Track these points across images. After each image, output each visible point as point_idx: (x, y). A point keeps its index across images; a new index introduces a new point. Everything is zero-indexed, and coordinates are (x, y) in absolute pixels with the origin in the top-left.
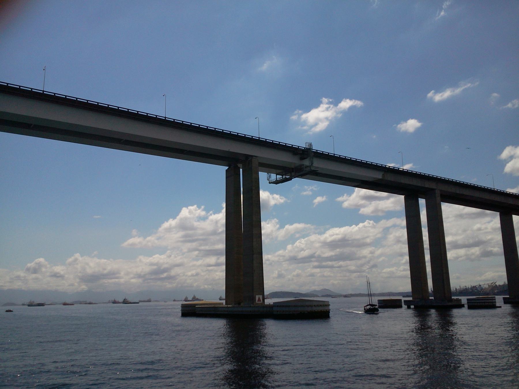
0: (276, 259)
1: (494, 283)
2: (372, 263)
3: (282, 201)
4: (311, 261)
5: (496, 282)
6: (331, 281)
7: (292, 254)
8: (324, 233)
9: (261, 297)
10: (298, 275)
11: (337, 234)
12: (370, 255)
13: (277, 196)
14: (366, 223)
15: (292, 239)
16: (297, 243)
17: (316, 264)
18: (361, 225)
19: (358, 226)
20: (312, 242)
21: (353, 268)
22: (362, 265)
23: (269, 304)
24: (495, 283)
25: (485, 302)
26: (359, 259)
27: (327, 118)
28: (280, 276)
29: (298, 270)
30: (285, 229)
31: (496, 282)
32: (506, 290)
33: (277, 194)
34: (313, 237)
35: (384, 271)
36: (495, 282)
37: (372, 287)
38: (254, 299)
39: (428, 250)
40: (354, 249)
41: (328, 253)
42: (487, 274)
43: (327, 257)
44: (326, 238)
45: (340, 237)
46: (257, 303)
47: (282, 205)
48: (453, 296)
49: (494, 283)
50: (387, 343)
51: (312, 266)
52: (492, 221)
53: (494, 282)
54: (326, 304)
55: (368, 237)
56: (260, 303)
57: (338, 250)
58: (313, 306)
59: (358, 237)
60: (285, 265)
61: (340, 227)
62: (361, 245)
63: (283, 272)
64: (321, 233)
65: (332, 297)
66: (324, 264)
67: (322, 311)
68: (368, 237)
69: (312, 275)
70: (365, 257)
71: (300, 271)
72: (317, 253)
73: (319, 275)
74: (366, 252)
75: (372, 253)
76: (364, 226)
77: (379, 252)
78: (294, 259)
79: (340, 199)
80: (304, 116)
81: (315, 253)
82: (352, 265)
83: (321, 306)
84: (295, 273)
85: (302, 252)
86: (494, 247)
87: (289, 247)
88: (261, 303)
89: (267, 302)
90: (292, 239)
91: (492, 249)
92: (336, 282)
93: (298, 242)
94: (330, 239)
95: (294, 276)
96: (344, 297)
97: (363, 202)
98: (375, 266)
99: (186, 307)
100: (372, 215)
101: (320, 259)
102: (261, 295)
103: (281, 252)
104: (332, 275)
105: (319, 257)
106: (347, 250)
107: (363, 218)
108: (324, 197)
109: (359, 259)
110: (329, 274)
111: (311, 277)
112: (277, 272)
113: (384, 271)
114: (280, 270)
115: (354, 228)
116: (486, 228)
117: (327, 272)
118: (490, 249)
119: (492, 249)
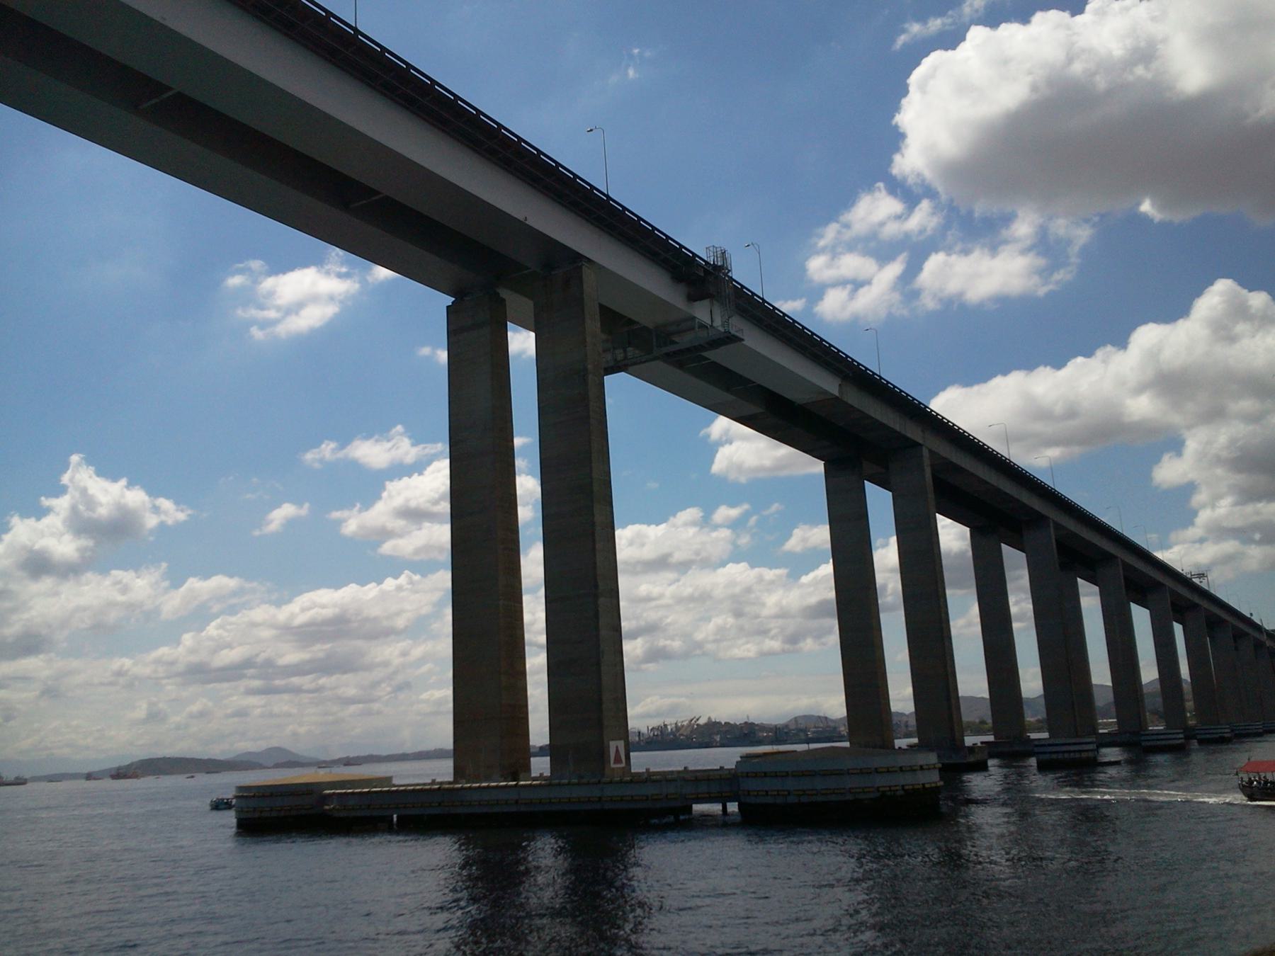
0: (147, 671)
1: (695, 720)
2: (400, 678)
3: (181, 516)
4: (242, 677)
5: (700, 717)
6: (291, 727)
7: (194, 659)
8: (289, 601)
9: (621, 744)
10: (202, 714)
11: (323, 607)
12: (402, 659)
13: (166, 504)
14: (403, 580)
15: (199, 616)
16: (212, 630)
17: (257, 683)
18: (390, 583)
19: (381, 586)
20: (254, 625)
21: (351, 692)
22: (375, 685)
23: (681, 769)
24: (698, 720)
25: (1080, 751)
26: (369, 668)
27: (331, 298)
28: (154, 716)
29: (204, 700)
30: (182, 589)
31: (700, 717)
32: (746, 734)
33: (167, 497)
34: (260, 613)
35: (424, 696)
36: (697, 717)
37: (750, 718)
38: (602, 754)
39: (532, 644)
40: (360, 643)
41: (292, 656)
42: (649, 700)
43: (286, 667)
44: (293, 616)
45: (328, 613)
46: (613, 769)
47: (179, 526)
48: (632, 751)
49: (695, 720)
50: (682, 884)
51: (242, 689)
52: (678, 580)
53: (695, 717)
54: (921, 763)
55: (398, 614)
56: (619, 768)
57: (318, 647)
58: (915, 770)
59: (375, 612)
60: (170, 688)
61: (337, 586)
62: (381, 632)
63: (161, 705)
64: (279, 603)
65: (320, 766)
66: (278, 682)
67: (927, 786)
68: (398, 614)
69: (242, 713)
70: (386, 664)
71: (210, 704)
72: (263, 656)
73: (258, 711)
74: (389, 652)
75: (404, 654)
76: (399, 588)
77: (418, 652)
78: (199, 673)
79: (336, 515)
80: (269, 283)
81: (257, 655)
82: (348, 685)
83: (922, 768)
84: (195, 708)
85: (225, 652)
86: (673, 639)
87: (188, 639)
88: (623, 768)
89: (641, 762)
90: (199, 616)
91: (668, 642)
92: (302, 730)
93: (213, 624)
94: (301, 619)
95: (191, 716)
96: (345, 765)
97: (401, 523)
98: (405, 686)
99: (272, 795)
100: (417, 558)
101: (268, 669)
102: (620, 739)
103: (164, 651)
104: (294, 711)
105: (269, 663)
106: (344, 647)
107: (395, 566)
108: (307, 505)
109: (369, 668)
110: (285, 708)
111: (236, 719)
112: (145, 706)
113: (424, 696)
114: (154, 699)
115: (371, 590)
116: (661, 596)
117: (282, 704)
118: (662, 643)
119: (668, 642)
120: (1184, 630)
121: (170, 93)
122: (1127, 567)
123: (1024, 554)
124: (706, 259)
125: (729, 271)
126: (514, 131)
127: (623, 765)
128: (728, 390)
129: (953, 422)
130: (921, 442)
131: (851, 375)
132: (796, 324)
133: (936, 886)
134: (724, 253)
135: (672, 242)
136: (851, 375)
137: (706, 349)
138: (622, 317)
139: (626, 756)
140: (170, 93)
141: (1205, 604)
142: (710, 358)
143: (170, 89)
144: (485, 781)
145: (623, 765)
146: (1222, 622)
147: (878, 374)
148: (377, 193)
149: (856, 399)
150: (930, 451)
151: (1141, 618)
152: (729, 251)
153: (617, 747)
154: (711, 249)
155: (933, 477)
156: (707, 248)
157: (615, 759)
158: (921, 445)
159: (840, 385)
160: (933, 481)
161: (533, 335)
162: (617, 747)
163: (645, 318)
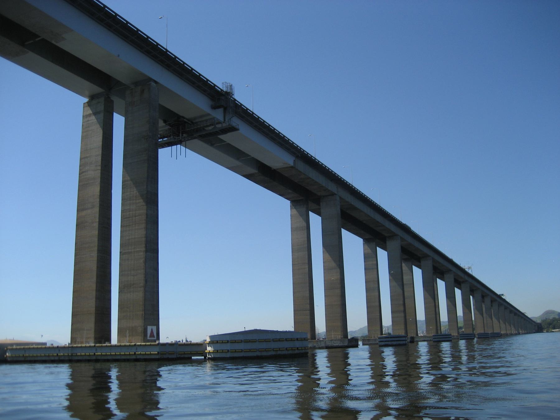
102: (154, 325)
120: (445, 283)
121: (39, 39)
122: (434, 260)
123: (320, 218)
124: (222, 88)
125: (233, 95)
126: (181, 59)
127: (148, 338)
128: (238, 159)
129: (357, 188)
130: (336, 193)
131: (300, 156)
132: (290, 141)
133: (549, 330)
134: (231, 86)
135: (255, 115)
136: (300, 156)
137: (220, 134)
138: (244, 153)
139: (157, 333)
140: (39, 39)
141: (470, 280)
142: (251, 155)
143: (39, 37)
144: (80, 344)
145: (148, 338)
146: (495, 300)
147: (314, 157)
148: (250, 156)
149: (302, 166)
150: (340, 198)
151: (441, 285)
152: (233, 85)
153: (152, 329)
154: (225, 83)
155: (341, 211)
156: (222, 83)
157: (151, 334)
158: (335, 194)
159: (294, 160)
160: (341, 212)
161: (124, 118)
162: (152, 329)
163: (188, 114)
